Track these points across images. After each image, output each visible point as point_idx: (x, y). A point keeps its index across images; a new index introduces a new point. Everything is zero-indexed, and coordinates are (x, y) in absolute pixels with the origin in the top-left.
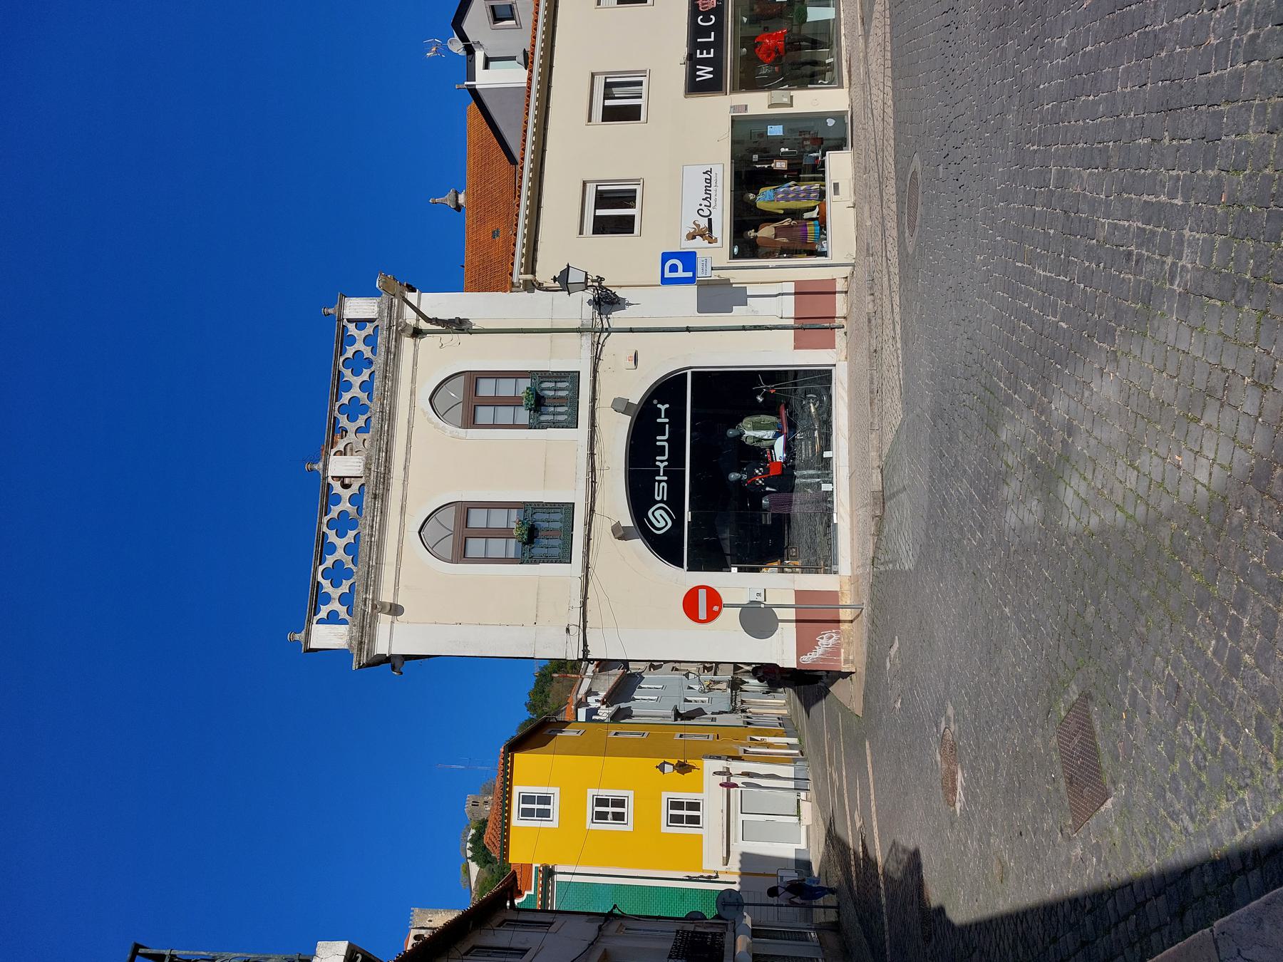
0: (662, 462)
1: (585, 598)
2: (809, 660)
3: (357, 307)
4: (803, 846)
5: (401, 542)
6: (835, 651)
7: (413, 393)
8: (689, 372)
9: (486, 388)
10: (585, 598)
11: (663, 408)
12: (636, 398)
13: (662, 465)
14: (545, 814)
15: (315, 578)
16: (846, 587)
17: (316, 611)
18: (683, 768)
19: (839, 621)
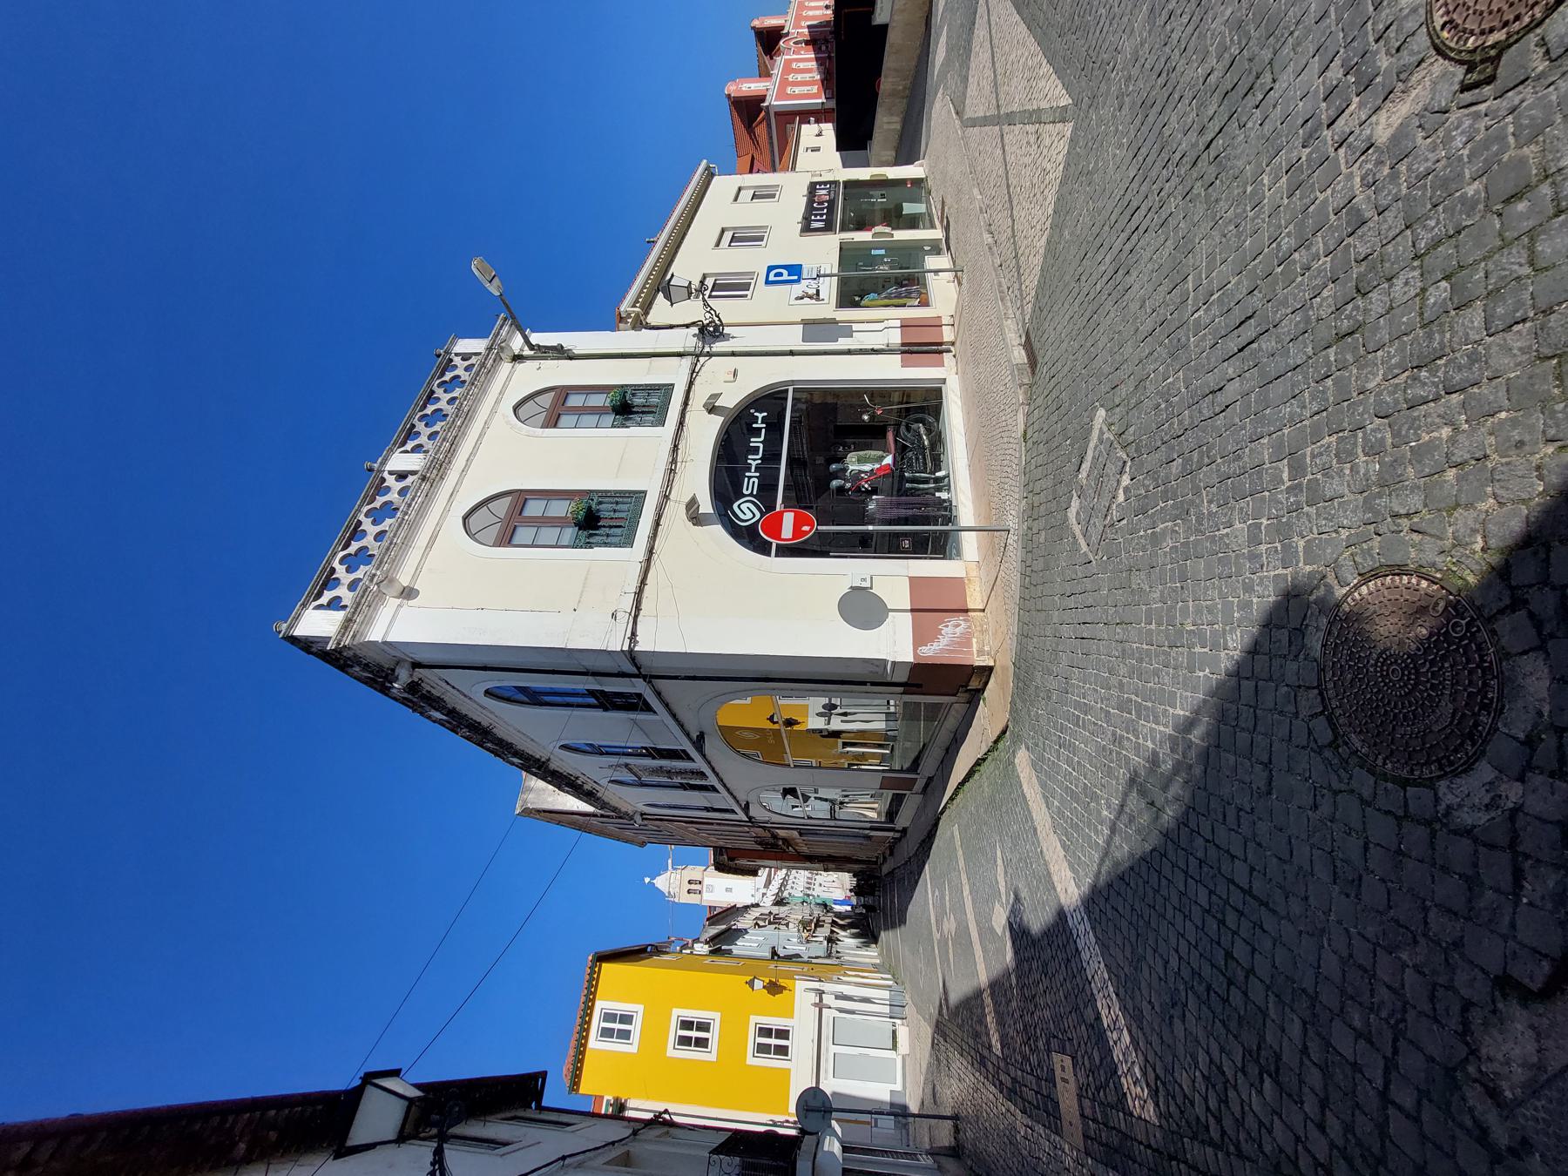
0: (754, 461)
1: (643, 582)
2: (932, 652)
3: (464, 345)
4: (898, 1087)
5: (439, 525)
6: (965, 641)
7: (502, 393)
8: (791, 389)
9: (575, 401)
10: (643, 582)
11: (760, 416)
12: (732, 398)
13: (754, 464)
14: (625, 1035)
15: (329, 562)
16: (974, 573)
17: (319, 595)
18: (774, 988)
19: (967, 611)
